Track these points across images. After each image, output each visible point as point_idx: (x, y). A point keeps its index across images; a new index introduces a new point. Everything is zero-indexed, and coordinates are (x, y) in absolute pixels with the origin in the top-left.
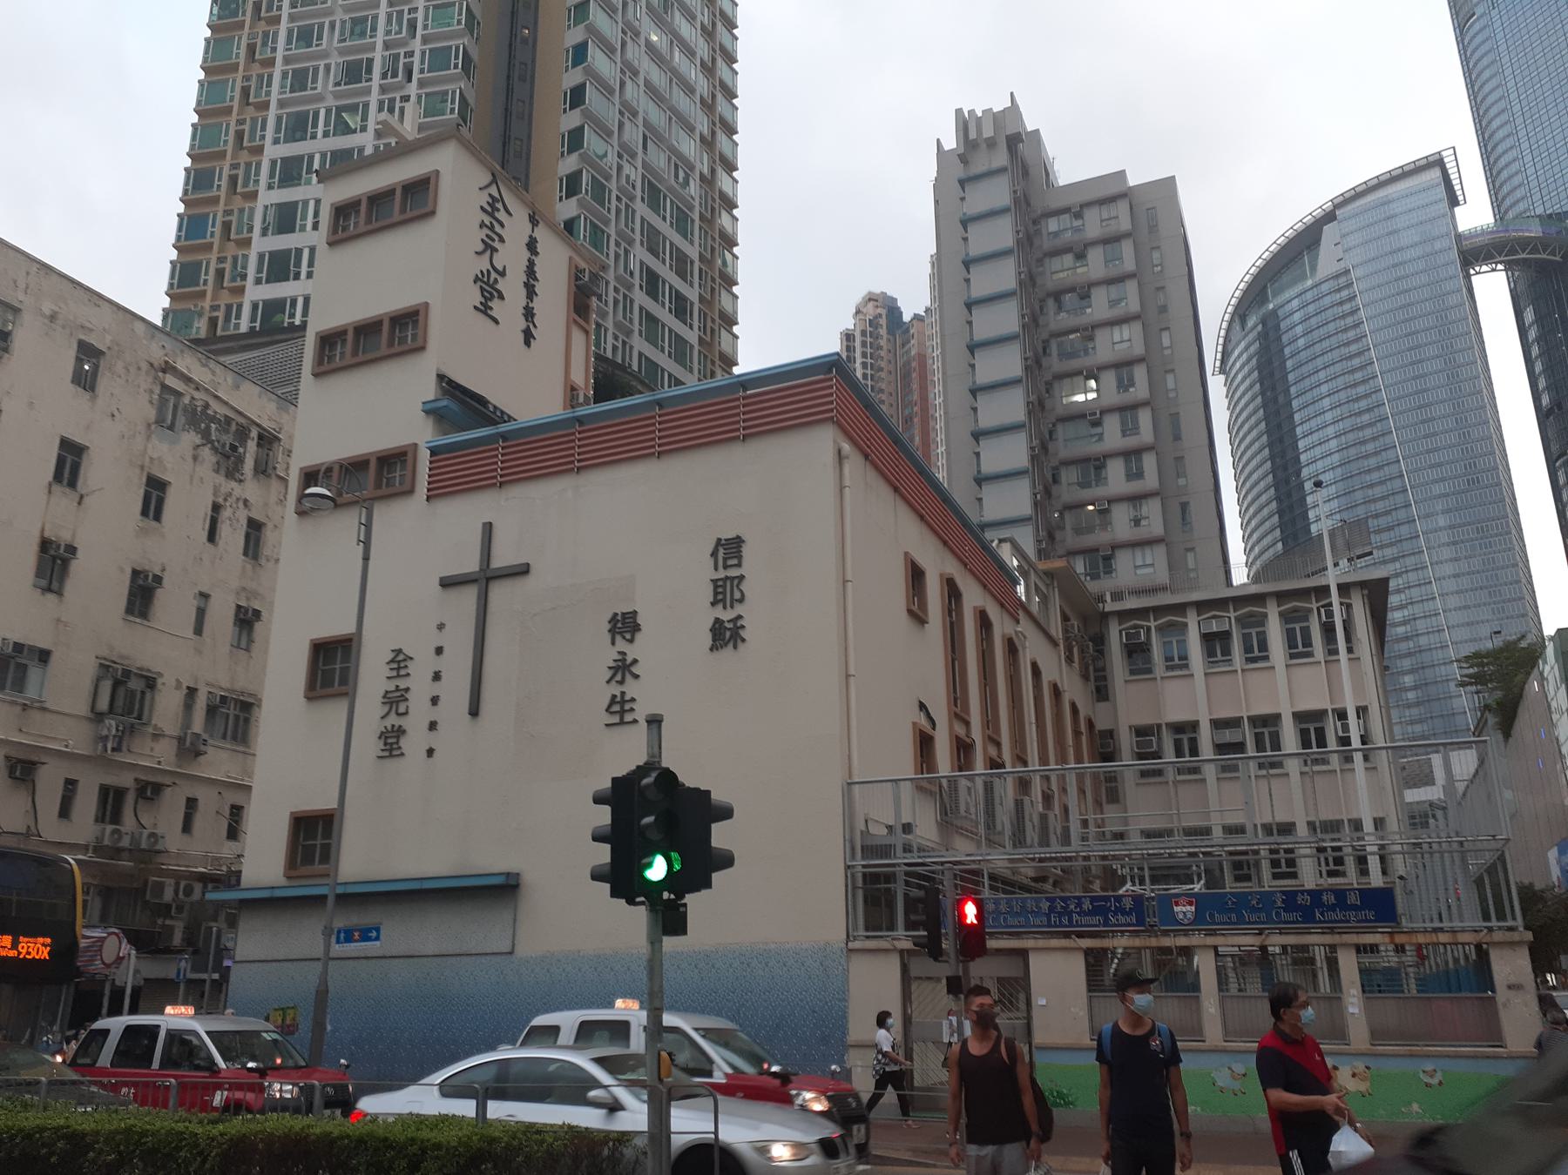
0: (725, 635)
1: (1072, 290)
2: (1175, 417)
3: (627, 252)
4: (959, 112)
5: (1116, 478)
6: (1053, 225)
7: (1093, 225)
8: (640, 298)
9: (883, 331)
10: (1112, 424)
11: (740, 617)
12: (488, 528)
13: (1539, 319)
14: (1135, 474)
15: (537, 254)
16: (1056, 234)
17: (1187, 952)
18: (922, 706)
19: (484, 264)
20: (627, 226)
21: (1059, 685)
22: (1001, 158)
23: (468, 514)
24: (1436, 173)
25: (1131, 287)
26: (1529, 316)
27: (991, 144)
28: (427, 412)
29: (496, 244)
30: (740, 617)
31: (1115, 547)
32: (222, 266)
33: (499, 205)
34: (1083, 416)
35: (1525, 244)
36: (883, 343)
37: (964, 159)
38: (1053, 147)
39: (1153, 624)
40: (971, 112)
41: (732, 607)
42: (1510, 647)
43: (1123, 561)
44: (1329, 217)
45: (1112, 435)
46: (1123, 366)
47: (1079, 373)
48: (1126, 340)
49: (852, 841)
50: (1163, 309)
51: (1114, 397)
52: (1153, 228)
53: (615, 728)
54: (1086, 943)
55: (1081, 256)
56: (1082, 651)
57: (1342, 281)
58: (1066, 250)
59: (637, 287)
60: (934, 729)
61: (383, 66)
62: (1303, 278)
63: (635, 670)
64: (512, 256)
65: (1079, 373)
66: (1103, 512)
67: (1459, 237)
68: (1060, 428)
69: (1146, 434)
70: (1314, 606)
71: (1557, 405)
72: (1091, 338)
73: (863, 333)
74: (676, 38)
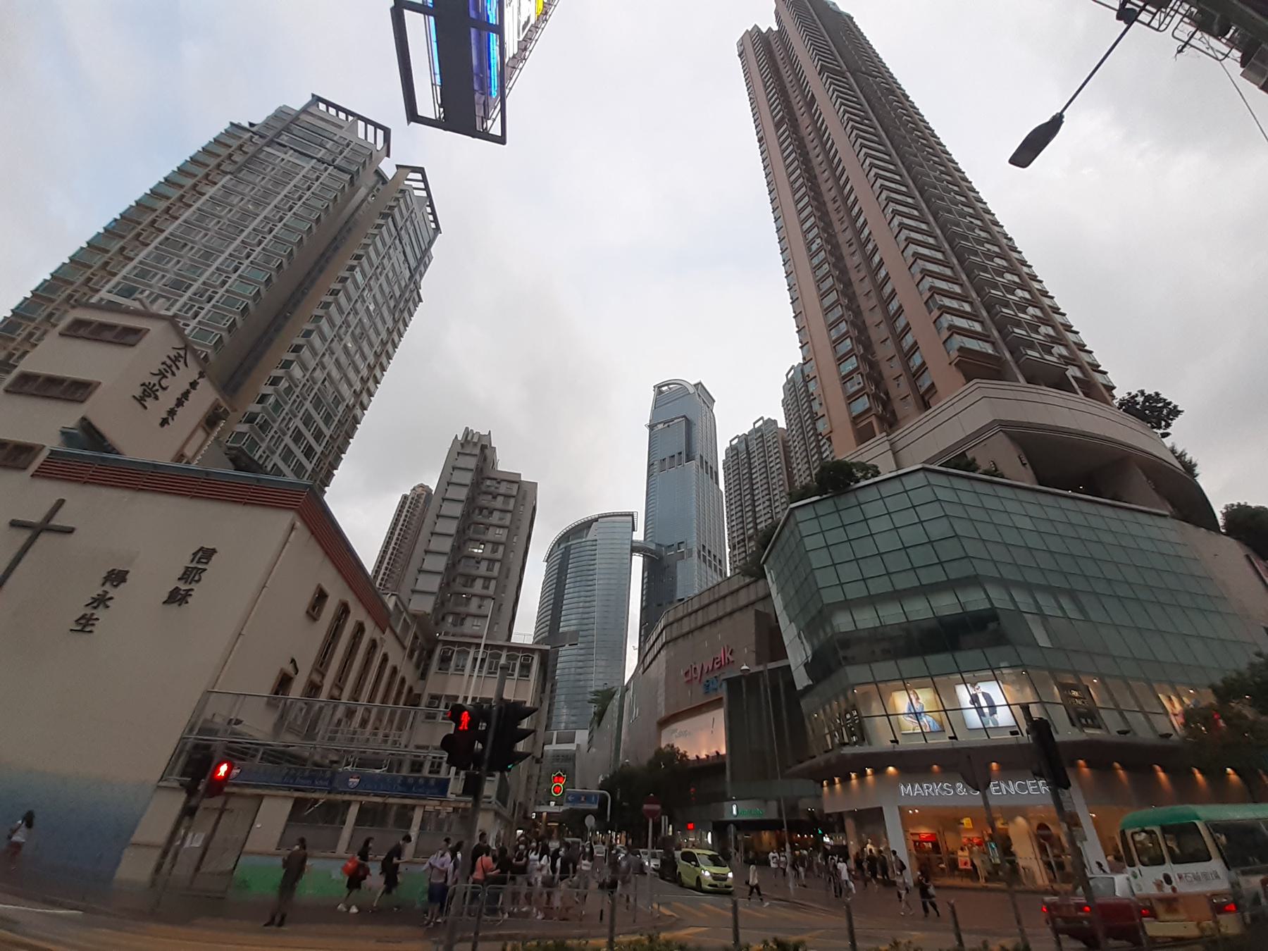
0: (177, 598)
1: (487, 508)
2: (509, 570)
3: (290, 419)
4: (467, 428)
5: (478, 587)
6: (488, 482)
7: (503, 488)
8: (288, 440)
9: (422, 501)
10: (484, 565)
11: (192, 590)
12: (61, 503)
13: (648, 577)
14: (486, 587)
15: (194, 389)
16: (489, 486)
17: (413, 808)
18: (293, 661)
19: (155, 380)
20: (297, 408)
21: (398, 668)
22: (477, 451)
23: (51, 491)
24: (630, 518)
25: (509, 515)
26: (646, 575)
27: (475, 444)
28: (63, 433)
29: (169, 375)
30: (192, 590)
31: (468, 615)
32: (35, 331)
33: (182, 360)
34: (474, 558)
35: (650, 550)
36: (420, 505)
37: (462, 445)
38: (499, 455)
39: (456, 649)
40: (472, 430)
41: (190, 583)
42: (609, 690)
43: (469, 621)
44: (596, 520)
45: (483, 569)
46: (496, 544)
47: (478, 541)
48: (500, 535)
49: (196, 723)
50: (518, 528)
51: (488, 554)
52: (524, 498)
53: (75, 633)
54: (297, 794)
55: (494, 498)
56: (420, 655)
57: (594, 543)
58: (490, 494)
59: (289, 435)
60: (296, 674)
61: (197, 289)
62: (582, 537)
63: (108, 603)
64: (177, 384)
65: (478, 541)
66: (468, 599)
67: (632, 541)
68: (463, 561)
69: (495, 573)
70: (521, 655)
71: (646, 606)
72: (488, 529)
73: (413, 498)
74: (360, 349)
